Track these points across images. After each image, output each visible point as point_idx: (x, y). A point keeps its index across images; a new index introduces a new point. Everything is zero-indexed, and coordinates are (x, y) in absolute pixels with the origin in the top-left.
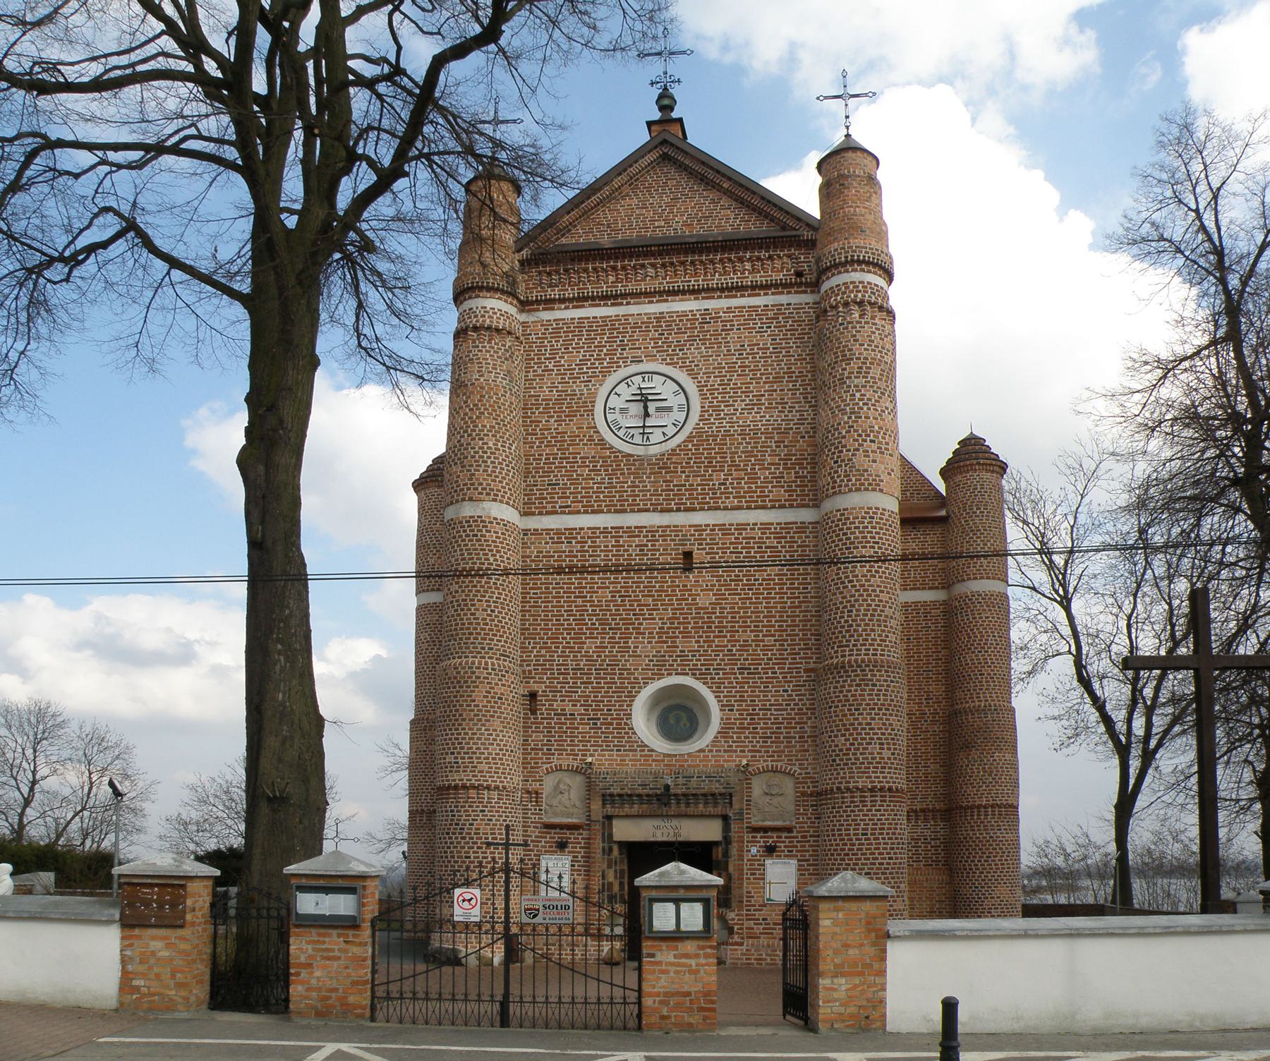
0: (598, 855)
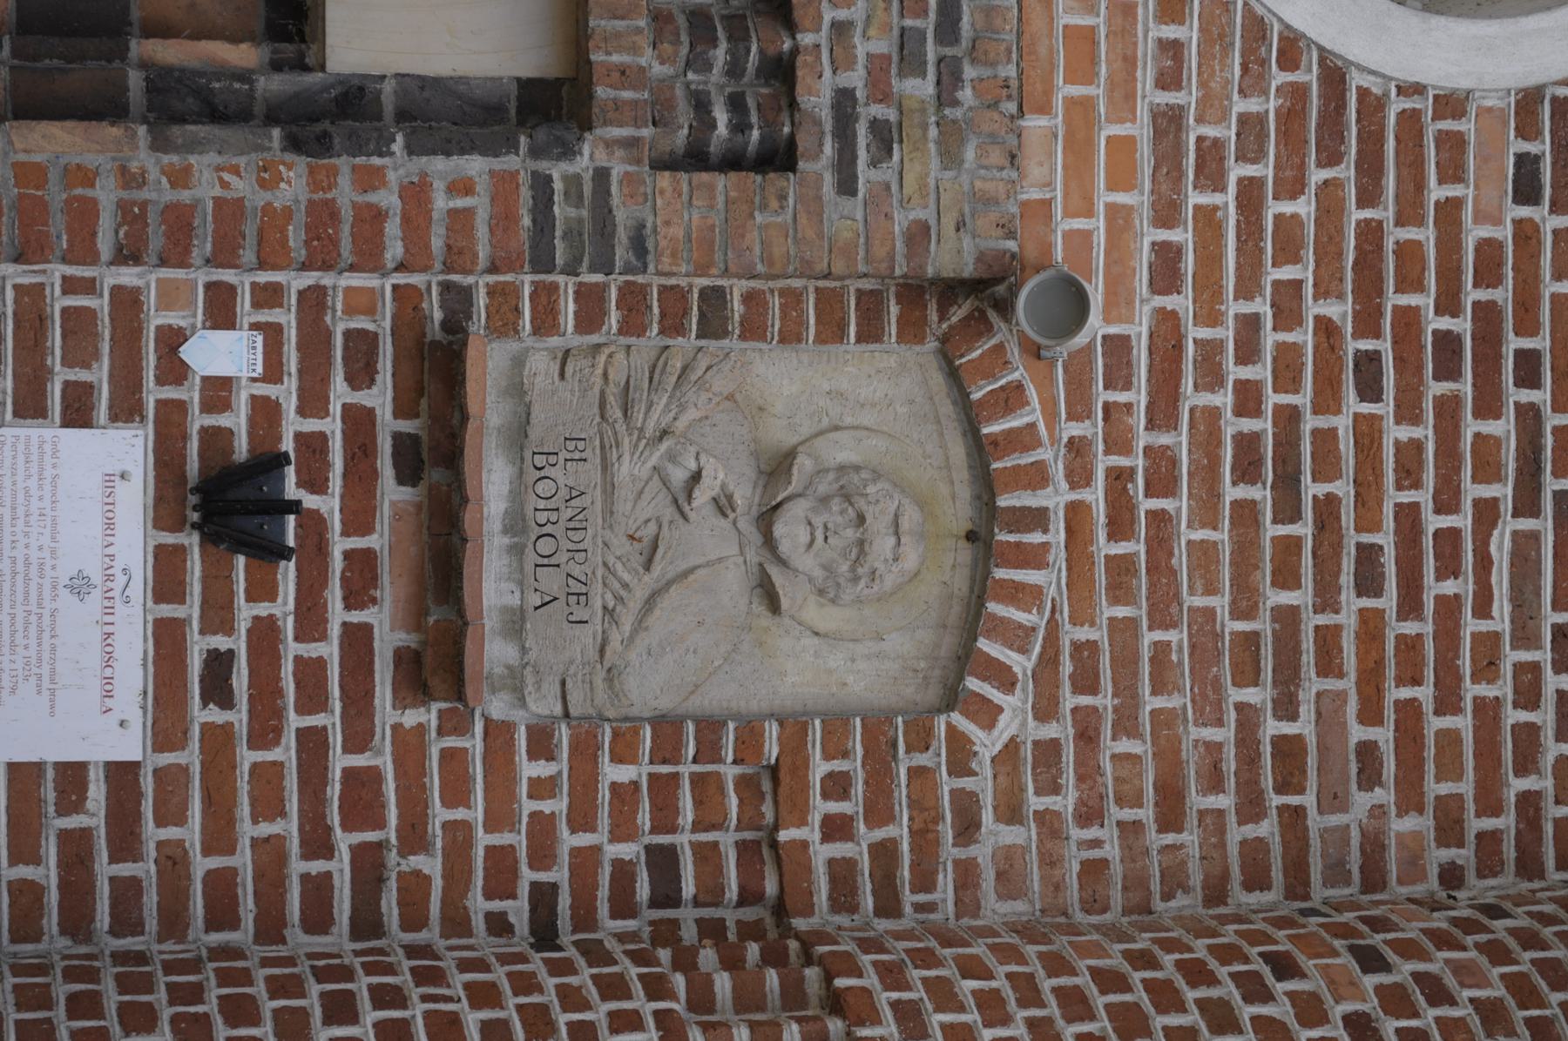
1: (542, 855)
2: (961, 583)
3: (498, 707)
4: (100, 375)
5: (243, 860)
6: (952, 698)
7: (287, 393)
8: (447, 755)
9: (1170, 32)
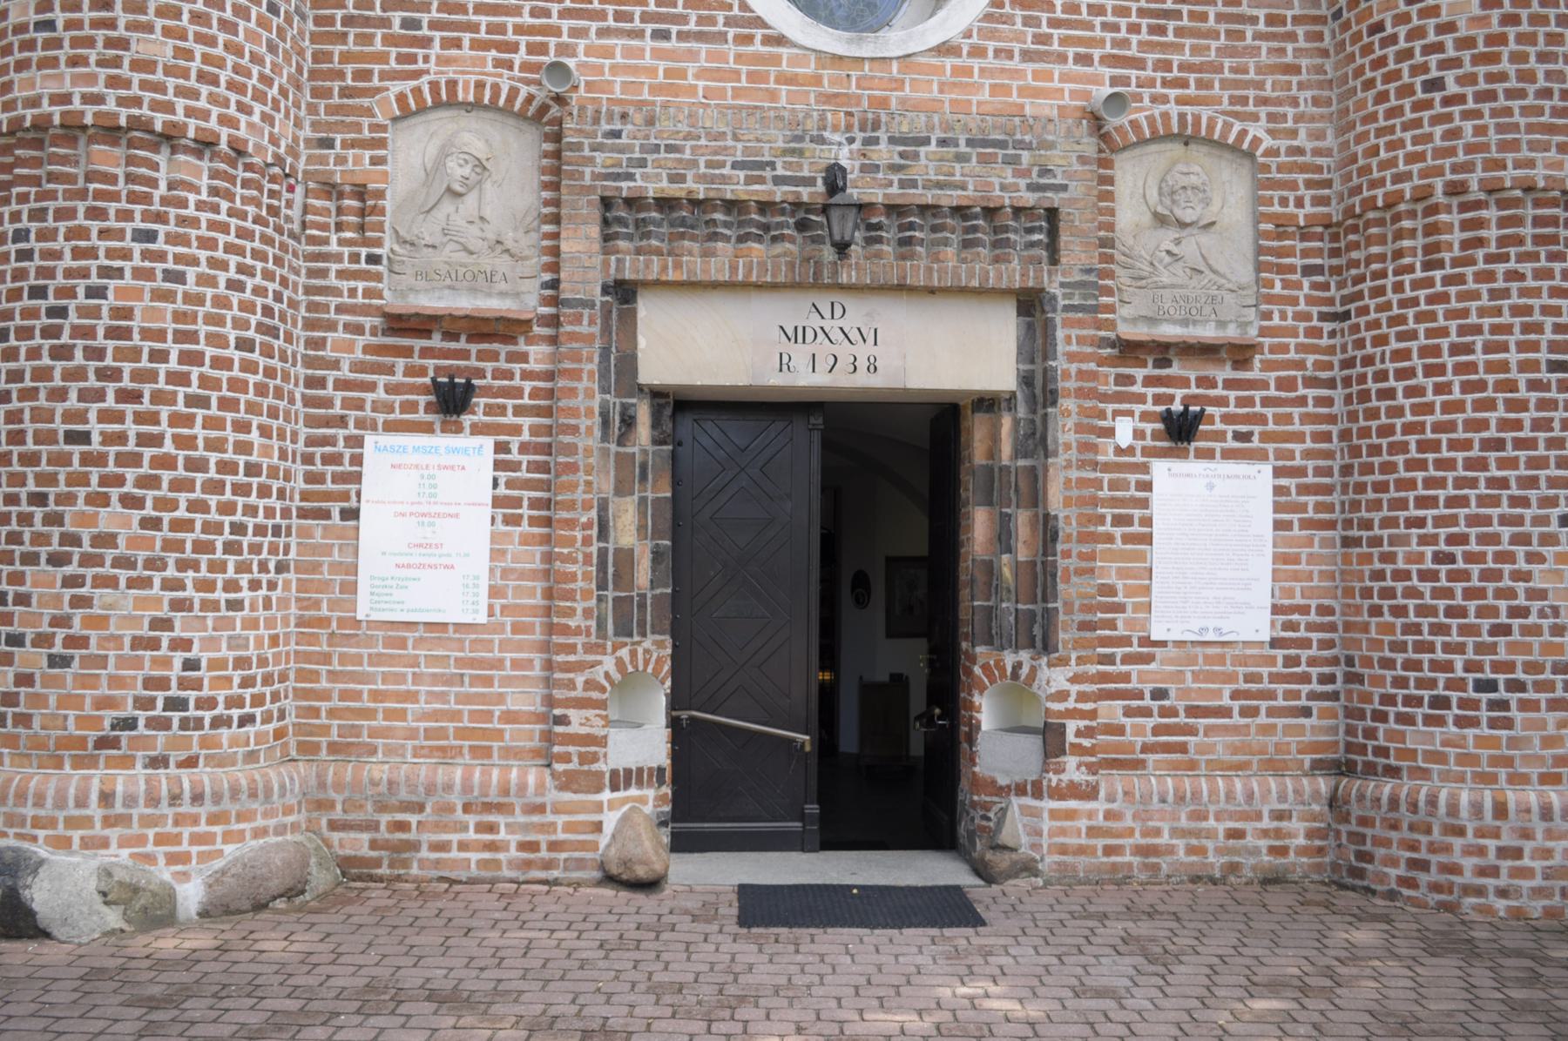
0: (588, 438)
1: (1307, 317)
2: (1204, 149)
3: (1253, 332)
4: (1133, 478)
5: (1308, 429)
6: (1250, 155)
7: (1138, 408)
8: (1271, 351)
9: (991, 53)
